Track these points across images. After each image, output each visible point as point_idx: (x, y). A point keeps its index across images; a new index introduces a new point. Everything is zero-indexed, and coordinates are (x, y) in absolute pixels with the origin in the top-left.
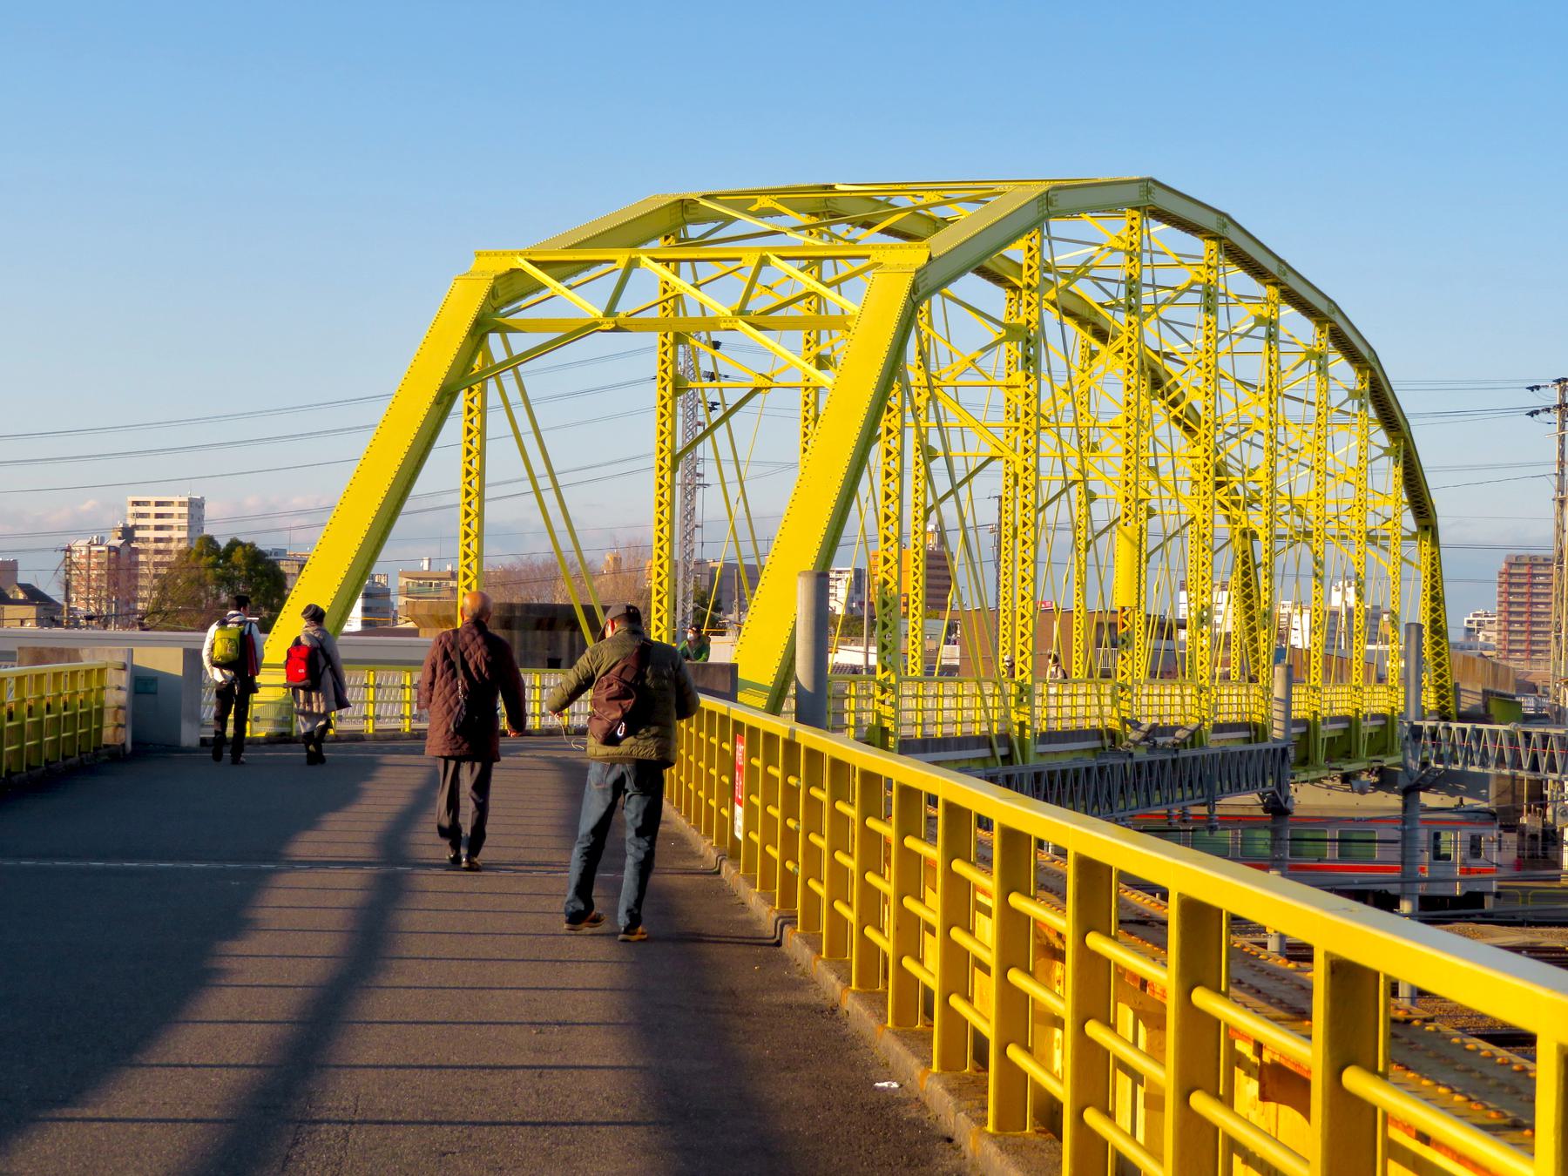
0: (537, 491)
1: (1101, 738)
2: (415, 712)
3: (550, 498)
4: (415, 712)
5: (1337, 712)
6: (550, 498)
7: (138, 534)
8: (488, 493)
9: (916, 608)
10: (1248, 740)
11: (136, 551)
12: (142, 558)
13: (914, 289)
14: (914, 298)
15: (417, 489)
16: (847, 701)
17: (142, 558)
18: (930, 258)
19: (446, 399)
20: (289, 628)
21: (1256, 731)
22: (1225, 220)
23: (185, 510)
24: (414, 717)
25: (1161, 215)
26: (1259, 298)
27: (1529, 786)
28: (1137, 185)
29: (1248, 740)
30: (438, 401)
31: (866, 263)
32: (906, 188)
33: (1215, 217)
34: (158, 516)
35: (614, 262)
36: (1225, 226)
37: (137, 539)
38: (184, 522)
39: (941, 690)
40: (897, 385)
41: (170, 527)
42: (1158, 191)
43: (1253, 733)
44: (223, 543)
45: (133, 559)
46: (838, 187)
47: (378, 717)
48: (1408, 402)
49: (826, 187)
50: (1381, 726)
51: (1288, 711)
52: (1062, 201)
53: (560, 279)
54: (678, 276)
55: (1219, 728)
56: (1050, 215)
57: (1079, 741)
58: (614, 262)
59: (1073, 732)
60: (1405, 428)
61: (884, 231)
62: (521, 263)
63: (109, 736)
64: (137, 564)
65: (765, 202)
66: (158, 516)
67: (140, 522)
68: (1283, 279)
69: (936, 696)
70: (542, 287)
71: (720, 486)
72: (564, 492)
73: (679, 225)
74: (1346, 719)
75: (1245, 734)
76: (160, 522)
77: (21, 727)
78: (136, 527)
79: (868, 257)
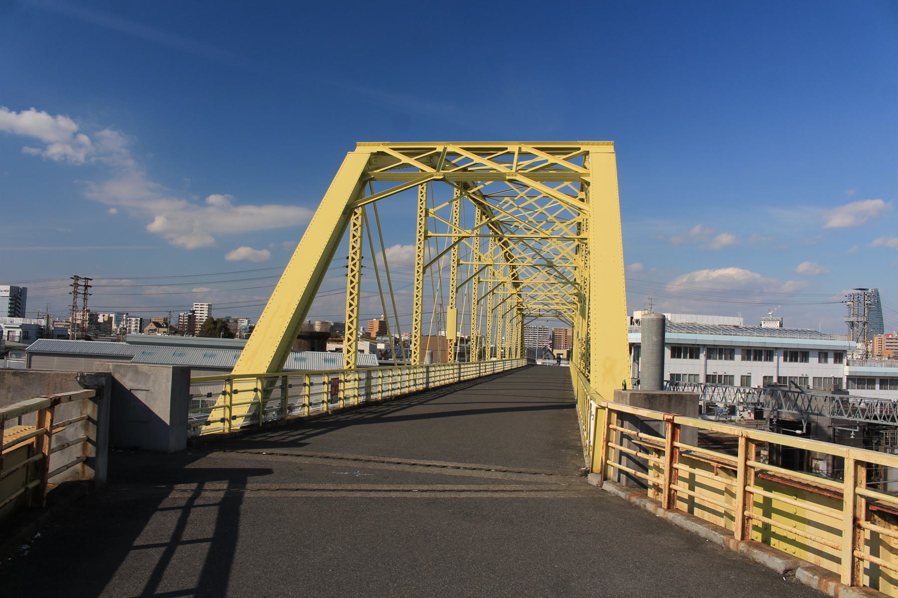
3: (387, 299)
6: (387, 299)
11: (195, 316)
23: (207, 307)
27: (680, 379)
30: (344, 213)
36: (11, 322)
38: (207, 309)
39: (391, 316)
41: (203, 311)
44: (215, 319)
64: (195, 322)
66: (201, 308)
67: (196, 309)
69: (414, 373)
71: (780, 366)
72: (391, 275)
76: (201, 315)
78: (196, 310)
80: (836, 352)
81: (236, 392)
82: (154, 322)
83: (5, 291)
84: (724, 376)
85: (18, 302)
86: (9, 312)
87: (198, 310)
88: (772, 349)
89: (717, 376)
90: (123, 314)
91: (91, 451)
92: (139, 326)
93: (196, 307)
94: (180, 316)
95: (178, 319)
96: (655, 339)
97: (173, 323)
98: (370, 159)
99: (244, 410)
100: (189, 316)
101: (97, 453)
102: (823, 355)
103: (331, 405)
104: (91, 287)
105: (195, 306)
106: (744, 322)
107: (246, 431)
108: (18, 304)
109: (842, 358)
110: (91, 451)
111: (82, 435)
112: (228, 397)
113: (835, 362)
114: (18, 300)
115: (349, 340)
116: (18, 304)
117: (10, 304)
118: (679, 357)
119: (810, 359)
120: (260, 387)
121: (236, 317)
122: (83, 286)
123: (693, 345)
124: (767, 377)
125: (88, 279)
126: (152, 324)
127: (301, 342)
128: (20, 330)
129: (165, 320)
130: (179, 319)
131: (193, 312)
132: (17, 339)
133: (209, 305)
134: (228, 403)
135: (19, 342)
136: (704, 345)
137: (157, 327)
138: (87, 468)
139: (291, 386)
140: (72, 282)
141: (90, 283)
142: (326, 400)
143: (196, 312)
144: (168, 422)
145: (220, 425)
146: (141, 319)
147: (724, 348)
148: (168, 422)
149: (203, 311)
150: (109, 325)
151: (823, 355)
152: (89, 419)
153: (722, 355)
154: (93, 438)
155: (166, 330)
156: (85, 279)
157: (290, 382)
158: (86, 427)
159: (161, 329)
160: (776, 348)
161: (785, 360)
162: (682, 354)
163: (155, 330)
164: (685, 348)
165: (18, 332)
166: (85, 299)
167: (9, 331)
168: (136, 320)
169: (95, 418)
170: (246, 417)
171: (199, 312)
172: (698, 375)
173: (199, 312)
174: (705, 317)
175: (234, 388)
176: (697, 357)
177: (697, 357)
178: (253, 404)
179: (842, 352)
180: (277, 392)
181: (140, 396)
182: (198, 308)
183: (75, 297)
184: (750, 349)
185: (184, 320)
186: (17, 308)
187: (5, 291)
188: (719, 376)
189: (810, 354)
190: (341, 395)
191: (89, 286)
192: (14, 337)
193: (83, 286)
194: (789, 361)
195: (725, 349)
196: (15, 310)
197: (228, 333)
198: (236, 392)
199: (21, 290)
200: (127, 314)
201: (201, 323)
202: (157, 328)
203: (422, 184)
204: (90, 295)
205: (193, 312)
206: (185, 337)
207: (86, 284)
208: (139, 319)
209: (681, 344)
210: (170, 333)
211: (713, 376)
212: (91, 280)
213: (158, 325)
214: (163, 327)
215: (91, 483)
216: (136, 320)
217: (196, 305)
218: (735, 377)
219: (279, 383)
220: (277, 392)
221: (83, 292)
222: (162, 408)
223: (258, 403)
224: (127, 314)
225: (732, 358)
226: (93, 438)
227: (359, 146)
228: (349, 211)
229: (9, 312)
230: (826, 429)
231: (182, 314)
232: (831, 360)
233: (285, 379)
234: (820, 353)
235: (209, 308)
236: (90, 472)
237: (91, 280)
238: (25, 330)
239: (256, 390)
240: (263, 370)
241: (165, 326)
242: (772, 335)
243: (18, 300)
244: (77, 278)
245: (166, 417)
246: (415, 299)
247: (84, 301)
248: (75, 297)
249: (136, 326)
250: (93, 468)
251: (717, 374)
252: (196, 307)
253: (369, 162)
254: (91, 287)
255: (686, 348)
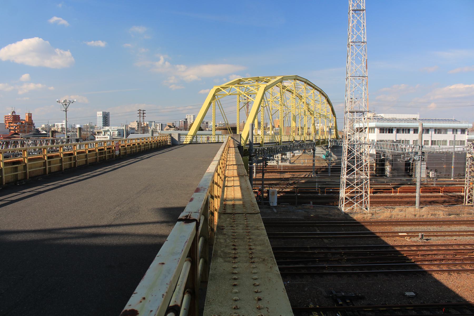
0: (222, 115)
5: (318, 139)
7: (187, 119)
8: (216, 115)
9: (262, 128)
10: (311, 142)
11: (187, 121)
12: (188, 122)
13: (265, 89)
17: (188, 122)
20: (45, 143)
23: (193, 116)
25: (298, 80)
29: (311, 142)
33: (305, 80)
34: (190, 117)
35: (230, 87)
38: (193, 118)
41: (191, 118)
46: (260, 77)
48: (332, 101)
51: (315, 138)
53: (224, 89)
54: (276, 86)
55: (307, 141)
58: (230, 87)
61: (264, 82)
62: (219, 87)
63: (168, 144)
64: (187, 124)
66: (190, 117)
67: (188, 118)
70: (222, 90)
74: (324, 139)
75: (310, 141)
76: (190, 121)
77: (149, 144)
80: (462, 129)
83: (100, 114)
84: (405, 140)
85: (106, 119)
86: (103, 124)
88: (429, 128)
89: (401, 141)
92: (161, 127)
97: (177, 126)
99: (189, 140)
100: (184, 122)
102: (455, 130)
104: (145, 113)
105: (187, 116)
106: (420, 117)
108: (106, 120)
109: (465, 132)
113: (462, 133)
114: (106, 118)
116: (106, 120)
117: (103, 120)
118: (383, 133)
119: (448, 132)
123: (390, 127)
124: (426, 141)
126: (167, 126)
128: (117, 131)
129: (173, 124)
131: (186, 119)
132: (116, 135)
135: (117, 136)
136: (395, 127)
139: (198, 137)
140: (138, 112)
143: (187, 119)
145: (185, 142)
146: (162, 124)
147: (405, 128)
149: (191, 118)
151: (455, 130)
153: (436, 131)
155: (174, 129)
157: (197, 137)
160: (431, 128)
161: (435, 133)
162: (385, 131)
164: (389, 129)
165: (116, 132)
167: (113, 132)
172: (409, 140)
174: (400, 115)
176: (392, 132)
177: (392, 132)
179: (465, 129)
180: (195, 138)
183: (140, 118)
184: (384, 128)
186: (106, 122)
187: (100, 114)
188: (402, 140)
189: (448, 130)
190: (210, 140)
192: (115, 134)
194: (437, 133)
195: (406, 129)
196: (105, 123)
199: (107, 113)
200: (154, 122)
203: (238, 87)
205: (186, 119)
209: (401, 127)
211: (399, 140)
213: (170, 127)
214: (173, 128)
216: (160, 125)
218: (410, 141)
219: (195, 137)
220: (195, 138)
221: (142, 116)
224: (154, 122)
225: (409, 132)
229: (103, 124)
230: (178, 127)
231: (181, 121)
232: (459, 133)
233: (196, 136)
234: (453, 130)
235: (194, 117)
238: (119, 132)
242: (440, 122)
243: (106, 118)
244: (140, 110)
245: (177, 140)
246: (261, 115)
248: (140, 118)
249: (160, 128)
251: (401, 140)
254: (145, 113)
255: (386, 129)
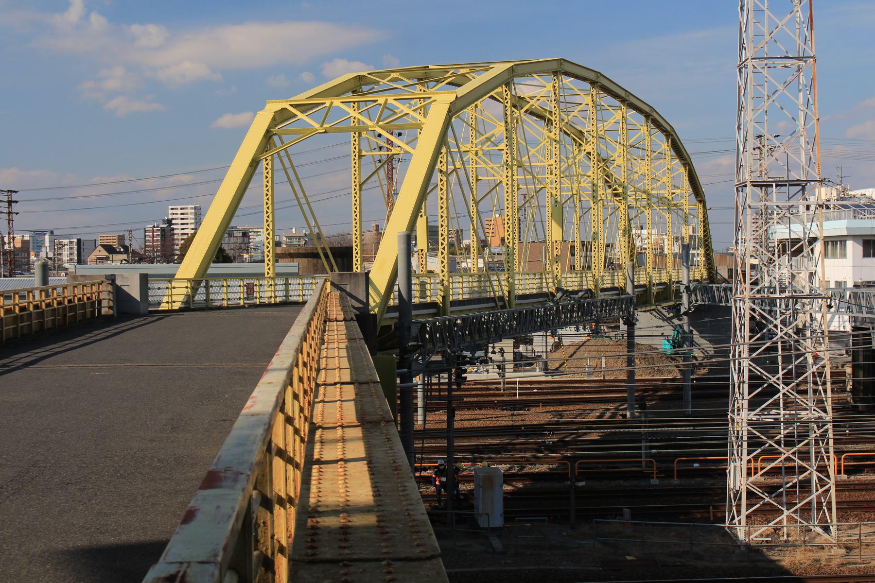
1: (548, 296)
2: (246, 296)
4: (246, 296)
7: (173, 222)
10: (618, 295)
11: (173, 229)
12: (175, 232)
13: (449, 111)
14: (450, 114)
15: (242, 205)
16: (427, 286)
18: (457, 97)
19: (254, 164)
21: (621, 290)
22: (599, 75)
24: (245, 298)
26: (617, 107)
28: (556, 62)
29: (618, 295)
30: (251, 165)
31: (430, 100)
32: (452, 66)
35: (325, 103)
36: (598, 77)
37: (173, 224)
38: (193, 216)
40: (444, 150)
41: (187, 219)
42: (566, 64)
43: (621, 291)
45: (172, 232)
46: (431, 67)
47: (229, 299)
48: (689, 148)
49: (425, 67)
50: (644, 291)
51: (633, 282)
52: (519, 70)
53: (302, 112)
56: (514, 76)
57: (484, 303)
59: (468, 300)
60: (688, 159)
63: (104, 311)
64: (174, 234)
65: (394, 75)
67: (174, 216)
68: (627, 98)
70: (295, 116)
73: (511, 77)
76: (183, 216)
78: (173, 219)
79: (431, 98)
81: (174, 288)
82: (103, 246)
87: (176, 219)
90: (42, 233)
91: (111, 304)
92: (76, 252)
93: (173, 214)
94: (145, 231)
95: (143, 231)
96: (402, 246)
98: (274, 116)
99: (181, 298)
100: (163, 230)
101: (113, 304)
103: (246, 301)
104: (16, 202)
105: (170, 212)
107: (181, 310)
110: (111, 304)
111: (107, 297)
112: (170, 290)
115: (442, 253)
120: (189, 286)
121: (247, 227)
122: (6, 202)
125: (11, 191)
126: (100, 248)
127: (317, 263)
129: (121, 238)
130: (146, 241)
131: (169, 222)
133: (195, 208)
134: (170, 294)
137: (110, 254)
138: (110, 310)
141: (14, 197)
142: (242, 297)
143: (173, 222)
144: (139, 300)
146: (79, 241)
148: (139, 300)
149: (187, 219)
150: (25, 255)
152: (110, 292)
154: (112, 299)
155: (125, 256)
156: (9, 191)
157: (210, 284)
158: (109, 295)
159: (116, 257)
163: (107, 258)
166: (10, 220)
168: (71, 242)
169: (112, 291)
170: (182, 302)
171: (180, 222)
173: (180, 222)
175: (173, 286)
178: (186, 295)
181: (125, 288)
182: (177, 214)
185: (153, 237)
191: (14, 202)
193: (6, 202)
197: (223, 256)
198: (174, 288)
200: (52, 233)
201: (185, 237)
202: (111, 256)
203: (354, 102)
204: (17, 213)
205: (169, 222)
206: (155, 265)
207: (8, 198)
208: (76, 240)
210: (132, 261)
212: (16, 192)
213: (110, 249)
214: (120, 253)
215: (112, 315)
217: (172, 209)
219: (203, 284)
220: (202, 290)
222: (136, 293)
223: (189, 295)
224: (52, 233)
226: (112, 299)
227: (269, 103)
228: (255, 163)
231: (149, 227)
236: (111, 312)
237: (16, 192)
239: (187, 287)
240: (192, 276)
241: (122, 250)
247: (9, 223)
250: (112, 310)
252: (173, 214)
253: (274, 119)
254: (16, 202)
